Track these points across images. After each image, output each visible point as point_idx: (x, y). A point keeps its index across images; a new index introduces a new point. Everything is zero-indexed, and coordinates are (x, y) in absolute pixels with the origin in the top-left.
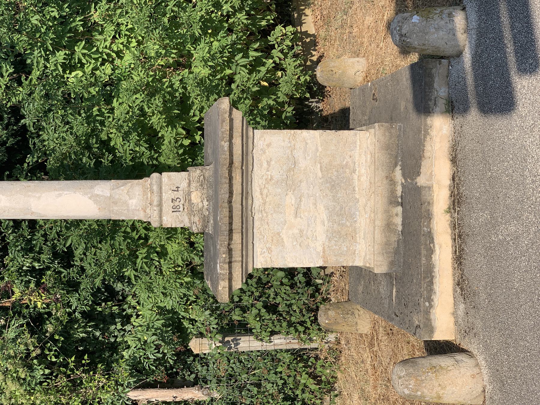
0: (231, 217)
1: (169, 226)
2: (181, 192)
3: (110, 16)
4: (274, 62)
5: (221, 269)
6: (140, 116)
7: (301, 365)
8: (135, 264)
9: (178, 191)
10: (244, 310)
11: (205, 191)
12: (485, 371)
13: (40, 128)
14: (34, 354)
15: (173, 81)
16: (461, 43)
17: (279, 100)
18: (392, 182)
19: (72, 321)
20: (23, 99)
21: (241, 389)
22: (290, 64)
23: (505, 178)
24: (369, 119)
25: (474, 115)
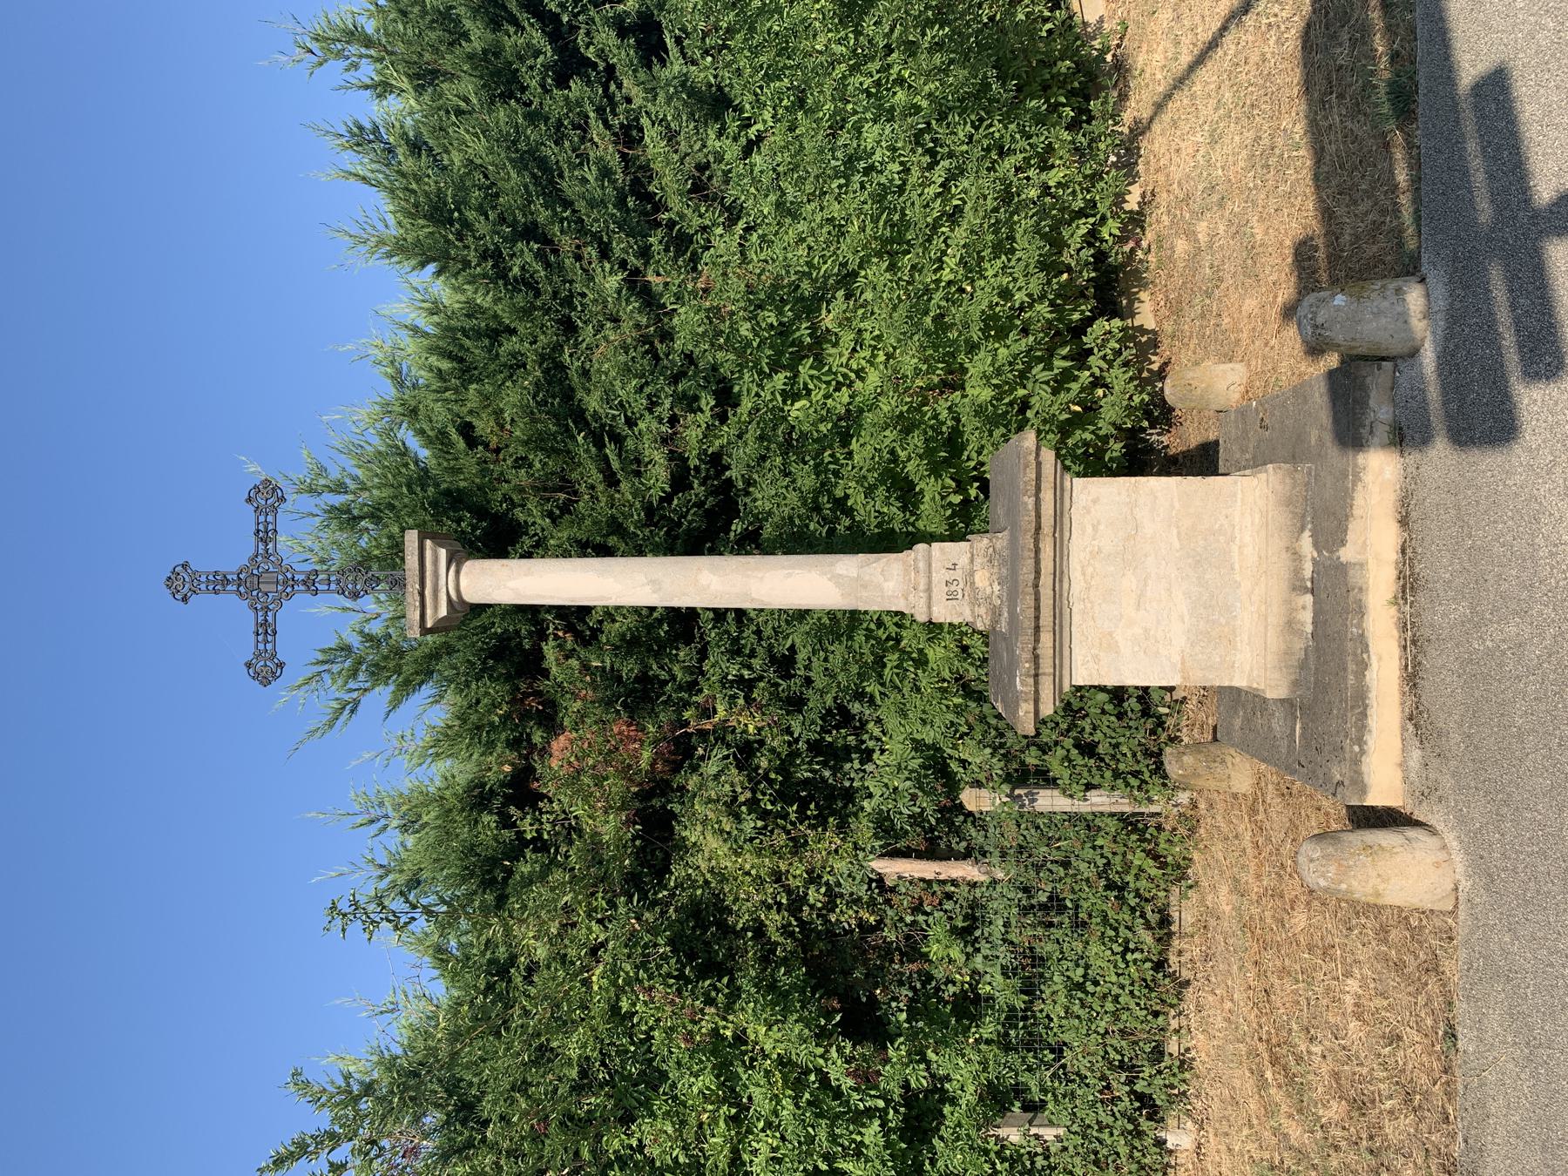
0: (1037, 608)
3: (848, 319)
4: (1092, 375)
5: (1022, 684)
6: (890, 461)
7: (1134, 837)
8: (881, 676)
10: (1044, 749)
12: (1458, 858)
13: (749, 483)
14: (742, 799)
15: (939, 409)
16: (1419, 335)
17: (1101, 433)
18: (1296, 556)
19: (794, 754)
20: (729, 443)
21: (1038, 868)
22: (1118, 377)
23: (1497, 549)
24: (1254, 458)
25: (1441, 449)
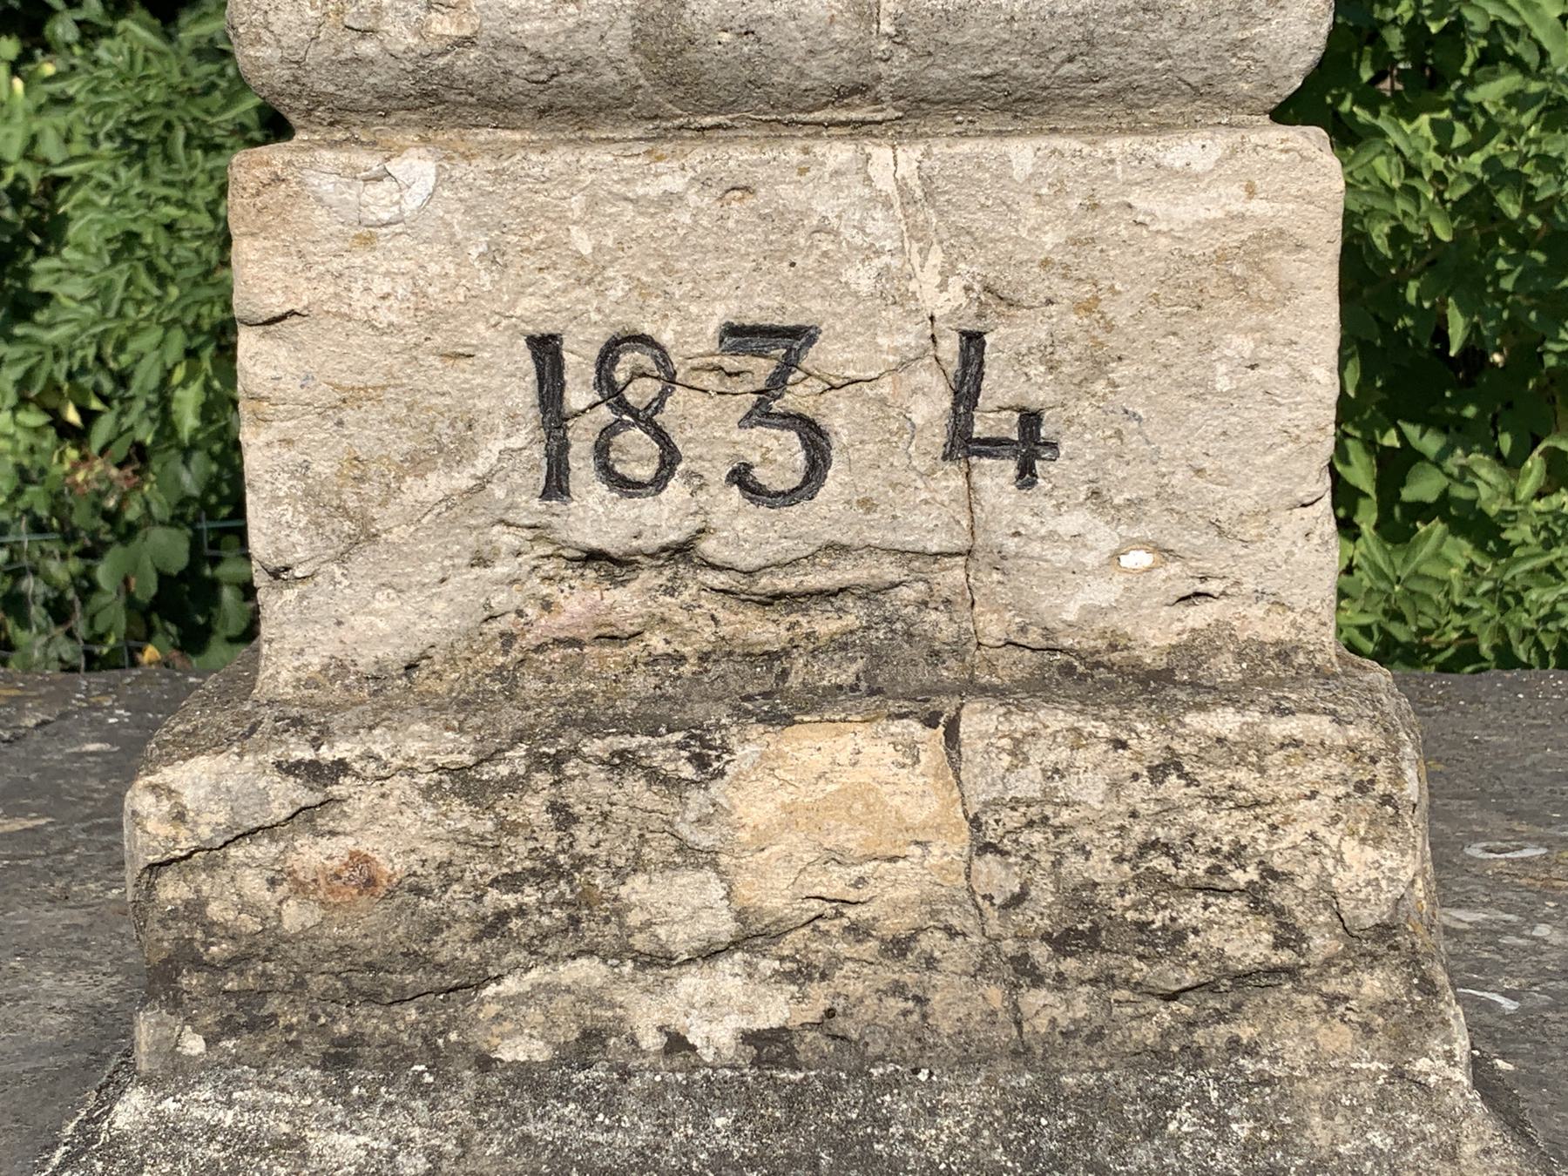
1: (259, 275)
2: (929, 505)
9: (964, 444)
11: (958, 1000)
